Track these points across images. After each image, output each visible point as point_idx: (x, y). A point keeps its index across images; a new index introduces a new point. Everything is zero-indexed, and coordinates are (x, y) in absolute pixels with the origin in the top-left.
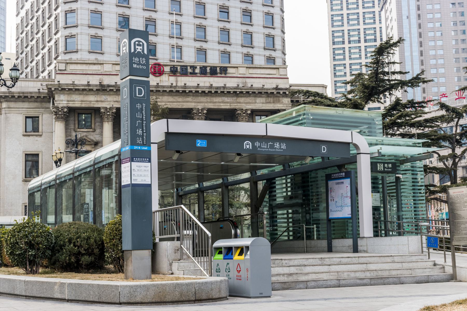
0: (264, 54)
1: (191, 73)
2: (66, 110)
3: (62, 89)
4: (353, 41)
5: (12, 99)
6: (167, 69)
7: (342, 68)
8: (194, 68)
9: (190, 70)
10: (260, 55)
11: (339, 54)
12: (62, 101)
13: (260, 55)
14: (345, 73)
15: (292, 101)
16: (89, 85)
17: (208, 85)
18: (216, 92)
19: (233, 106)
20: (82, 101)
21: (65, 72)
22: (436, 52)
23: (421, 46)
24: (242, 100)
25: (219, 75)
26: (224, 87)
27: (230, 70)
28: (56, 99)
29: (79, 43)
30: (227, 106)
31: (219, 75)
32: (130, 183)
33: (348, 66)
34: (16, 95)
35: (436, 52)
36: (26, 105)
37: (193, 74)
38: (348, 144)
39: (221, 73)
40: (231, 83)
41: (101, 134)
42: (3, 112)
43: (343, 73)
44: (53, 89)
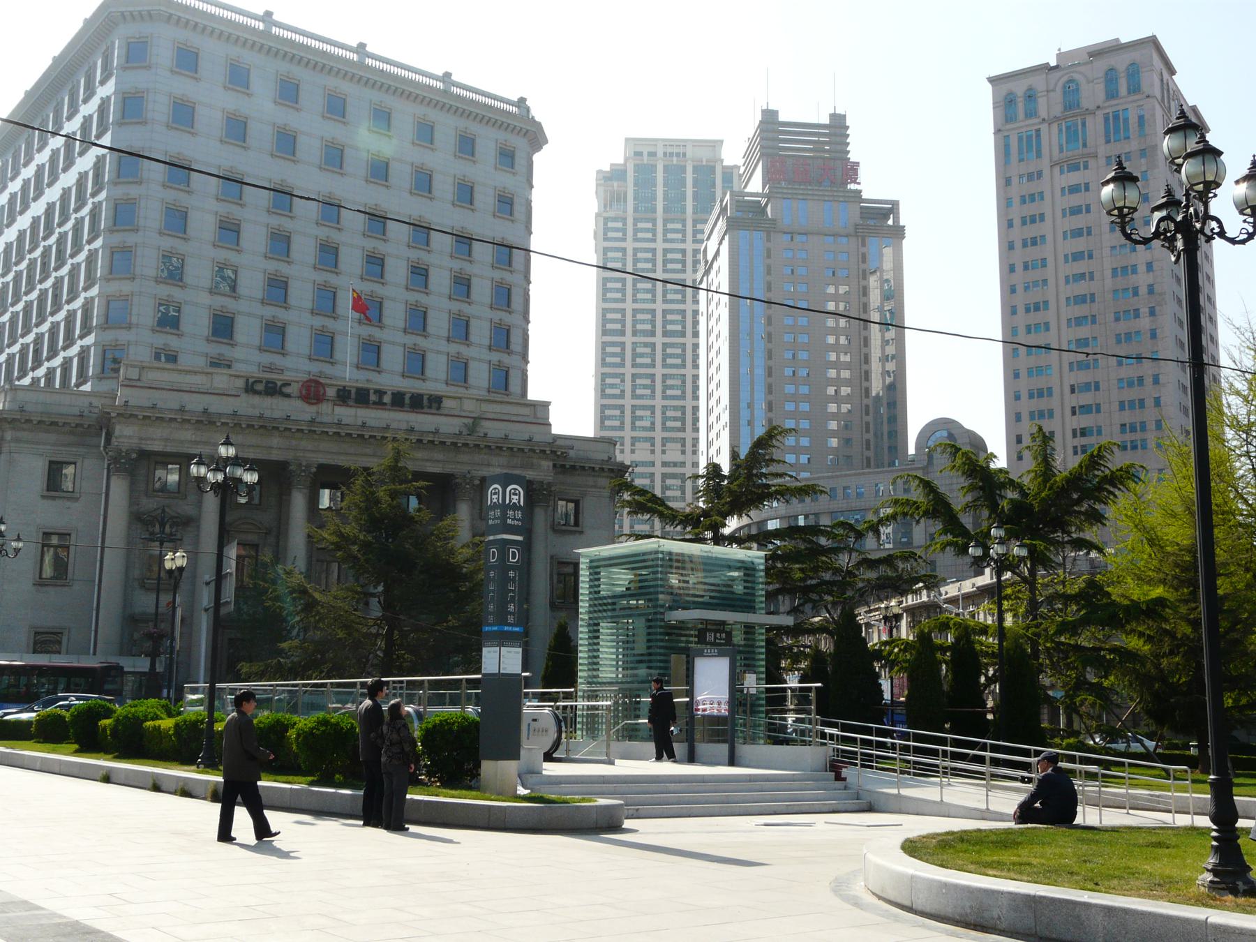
0: (488, 358)
1: (375, 403)
2: (134, 456)
3: (128, 415)
4: (641, 331)
5: (25, 426)
6: (331, 392)
7: (618, 381)
8: (381, 393)
9: (373, 397)
10: (480, 360)
11: (614, 355)
12: (127, 435)
13: (480, 360)
14: (623, 391)
15: (554, 466)
16: (182, 410)
17: (404, 426)
18: (420, 441)
19: (449, 469)
20: (167, 440)
21: (139, 384)
22: (797, 390)
23: (769, 256)
24: (464, 458)
25: (426, 410)
26: (436, 432)
27: (447, 403)
28: (117, 433)
29: (134, 311)
30: (436, 469)
31: (426, 410)
32: (153, 611)
33: (628, 378)
34: (35, 419)
35: (797, 390)
36: (52, 437)
37: (380, 404)
38: (1177, 812)
39: (430, 407)
40: (448, 425)
41: (199, 504)
42: (5, 449)
43: (617, 392)
44: (113, 415)
